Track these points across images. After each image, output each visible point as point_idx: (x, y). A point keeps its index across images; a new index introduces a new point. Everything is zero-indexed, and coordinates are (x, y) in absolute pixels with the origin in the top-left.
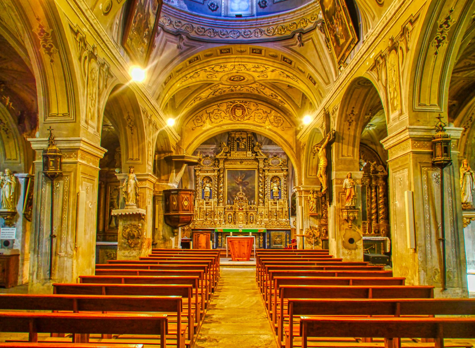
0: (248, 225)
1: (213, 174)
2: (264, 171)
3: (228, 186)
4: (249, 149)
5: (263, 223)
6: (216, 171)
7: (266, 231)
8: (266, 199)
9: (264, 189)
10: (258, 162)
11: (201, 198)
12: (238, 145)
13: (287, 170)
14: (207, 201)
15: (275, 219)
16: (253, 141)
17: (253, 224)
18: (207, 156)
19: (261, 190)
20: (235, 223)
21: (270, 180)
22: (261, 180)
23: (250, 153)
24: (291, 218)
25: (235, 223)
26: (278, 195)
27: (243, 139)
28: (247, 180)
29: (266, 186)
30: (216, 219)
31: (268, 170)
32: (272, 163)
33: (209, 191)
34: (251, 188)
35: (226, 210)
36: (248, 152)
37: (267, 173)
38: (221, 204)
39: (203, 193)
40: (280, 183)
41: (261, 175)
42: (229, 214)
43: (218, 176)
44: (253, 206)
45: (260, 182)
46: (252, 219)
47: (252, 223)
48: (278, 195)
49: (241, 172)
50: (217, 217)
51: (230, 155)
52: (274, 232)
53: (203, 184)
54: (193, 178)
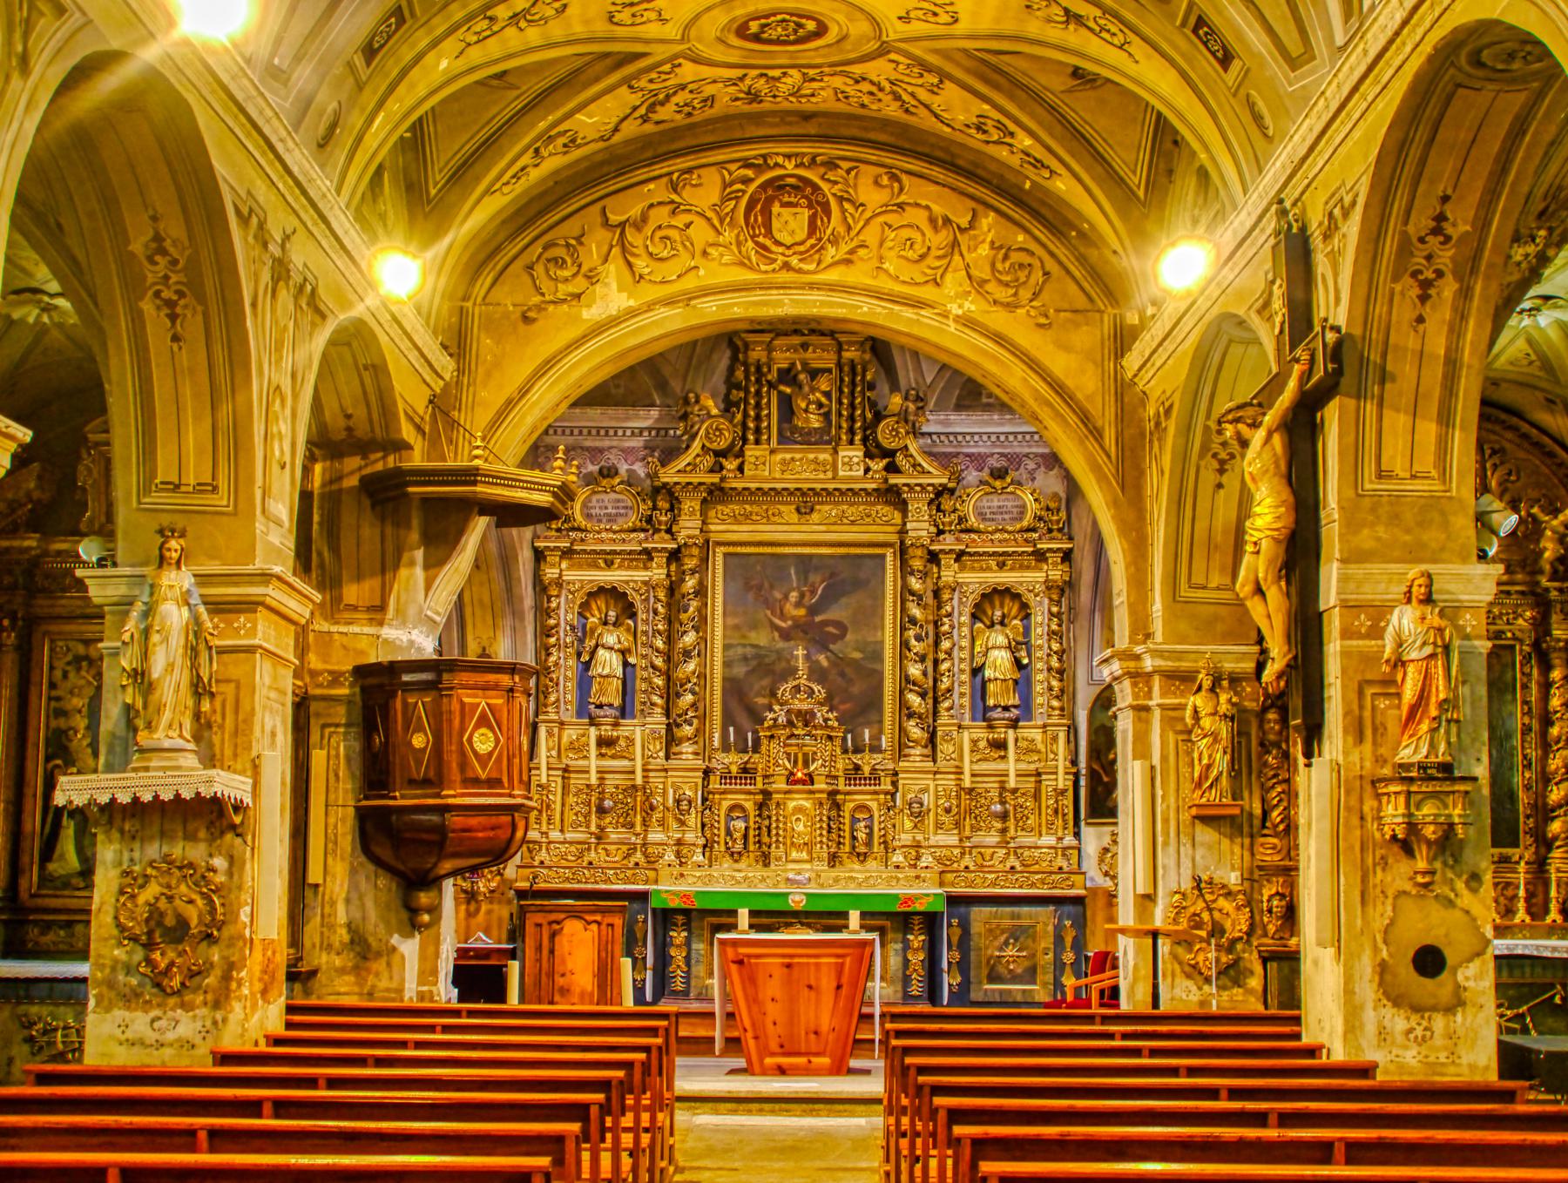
0: (838, 872)
1: (641, 575)
2: (933, 558)
3: (726, 647)
5: (926, 860)
6: (658, 559)
7: (941, 906)
8: (944, 718)
10: (902, 506)
11: (568, 715)
12: (787, 410)
13: (1067, 556)
14: (607, 731)
15: (993, 839)
16: (871, 387)
17: (872, 864)
18: (609, 472)
19: (915, 671)
20: (765, 860)
21: (967, 610)
22: (916, 612)
23: (857, 453)
24: (1088, 832)
25: (765, 860)
27: (814, 374)
29: (946, 645)
30: (655, 836)
31: (960, 556)
32: (981, 516)
33: (619, 672)
34: (857, 655)
35: (715, 784)
40: (1027, 631)
41: (915, 583)
42: (732, 808)
43: (672, 590)
44: (867, 761)
45: (913, 621)
46: (861, 836)
47: (863, 857)
49: (805, 563)
51: (741, 469)
52: (987, 910)
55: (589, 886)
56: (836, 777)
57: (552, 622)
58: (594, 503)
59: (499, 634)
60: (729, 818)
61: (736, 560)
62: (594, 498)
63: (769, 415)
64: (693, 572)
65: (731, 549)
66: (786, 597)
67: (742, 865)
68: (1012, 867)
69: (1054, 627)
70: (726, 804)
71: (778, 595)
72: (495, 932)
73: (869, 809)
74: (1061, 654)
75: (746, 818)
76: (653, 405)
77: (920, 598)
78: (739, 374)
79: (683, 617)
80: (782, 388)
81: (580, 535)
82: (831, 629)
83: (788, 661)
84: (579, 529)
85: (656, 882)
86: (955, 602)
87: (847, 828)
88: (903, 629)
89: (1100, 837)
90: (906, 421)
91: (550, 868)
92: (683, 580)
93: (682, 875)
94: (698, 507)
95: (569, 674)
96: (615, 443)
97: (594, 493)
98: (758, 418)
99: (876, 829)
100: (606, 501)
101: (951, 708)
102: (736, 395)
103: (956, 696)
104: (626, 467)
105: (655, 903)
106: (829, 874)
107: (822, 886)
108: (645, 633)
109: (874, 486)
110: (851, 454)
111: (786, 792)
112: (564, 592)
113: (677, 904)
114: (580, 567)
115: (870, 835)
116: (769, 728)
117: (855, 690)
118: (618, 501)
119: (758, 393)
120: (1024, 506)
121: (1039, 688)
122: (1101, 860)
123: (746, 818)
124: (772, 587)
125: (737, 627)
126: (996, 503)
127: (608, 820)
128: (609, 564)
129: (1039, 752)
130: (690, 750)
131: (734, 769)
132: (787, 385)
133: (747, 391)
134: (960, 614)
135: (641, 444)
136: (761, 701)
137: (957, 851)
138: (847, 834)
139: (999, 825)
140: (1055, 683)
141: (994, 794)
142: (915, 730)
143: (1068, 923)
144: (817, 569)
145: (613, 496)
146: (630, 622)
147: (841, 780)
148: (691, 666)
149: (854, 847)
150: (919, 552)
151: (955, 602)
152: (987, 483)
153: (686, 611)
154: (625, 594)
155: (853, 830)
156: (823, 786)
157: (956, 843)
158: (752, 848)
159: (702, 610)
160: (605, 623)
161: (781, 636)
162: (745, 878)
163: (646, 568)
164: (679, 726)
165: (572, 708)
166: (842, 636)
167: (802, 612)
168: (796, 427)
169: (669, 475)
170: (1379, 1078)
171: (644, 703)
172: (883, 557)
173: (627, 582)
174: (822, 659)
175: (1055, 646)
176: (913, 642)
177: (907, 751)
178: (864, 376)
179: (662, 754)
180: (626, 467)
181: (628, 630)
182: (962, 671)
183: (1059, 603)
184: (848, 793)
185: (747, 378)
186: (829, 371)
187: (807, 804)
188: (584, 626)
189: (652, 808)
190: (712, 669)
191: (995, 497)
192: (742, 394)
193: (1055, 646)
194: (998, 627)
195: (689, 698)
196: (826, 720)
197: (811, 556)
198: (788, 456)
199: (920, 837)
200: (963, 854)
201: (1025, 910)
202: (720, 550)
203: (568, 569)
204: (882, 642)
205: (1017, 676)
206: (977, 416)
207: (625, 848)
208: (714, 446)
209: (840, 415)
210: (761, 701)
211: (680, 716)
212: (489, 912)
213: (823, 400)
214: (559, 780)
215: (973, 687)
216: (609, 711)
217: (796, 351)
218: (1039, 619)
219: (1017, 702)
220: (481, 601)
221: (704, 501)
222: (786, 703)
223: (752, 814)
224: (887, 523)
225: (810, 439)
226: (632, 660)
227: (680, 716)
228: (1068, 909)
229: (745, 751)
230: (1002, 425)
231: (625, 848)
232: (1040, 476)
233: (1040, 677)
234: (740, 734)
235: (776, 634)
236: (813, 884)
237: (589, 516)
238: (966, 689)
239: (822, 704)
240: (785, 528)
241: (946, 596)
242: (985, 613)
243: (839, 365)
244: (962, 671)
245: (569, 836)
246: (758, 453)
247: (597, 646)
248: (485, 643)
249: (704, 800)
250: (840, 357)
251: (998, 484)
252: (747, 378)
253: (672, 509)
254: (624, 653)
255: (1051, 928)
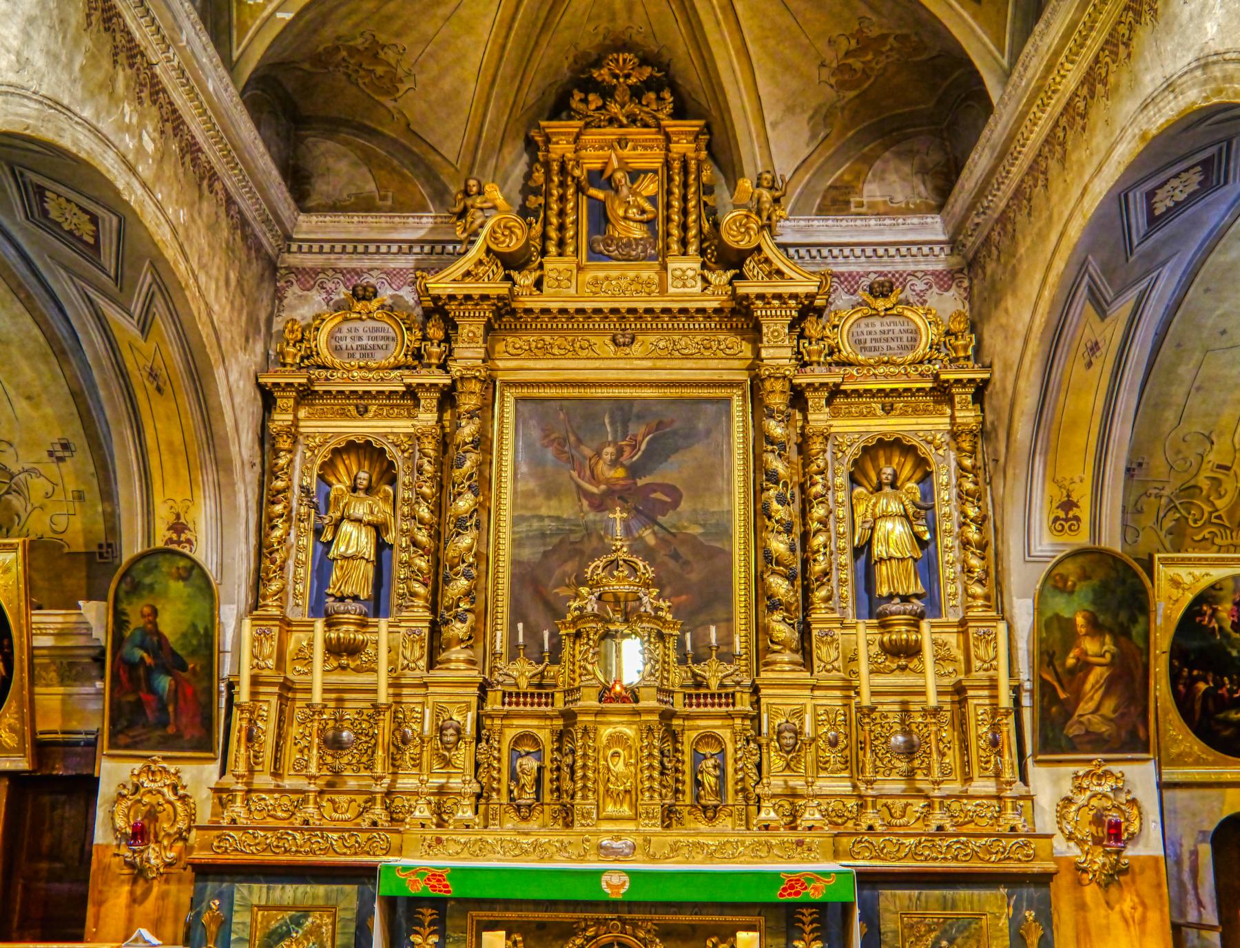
0: (674, 836)
1: (403, 426)
2: (798, 398)
3: (516, 521)
4: (684, 243)
5: (811, 816)
6: (429, 401)
7: (848, 893)
8: (819, 612)
9: (805, 537)
10: (754, 332)
11: (297, 611)
12: (600, 218)
13: (980, 392)
14: (347, 632)
15: (896, 786)
16: (709, 190)
17: (725, 823)
18: (363, 294)
19: (778, 545)
20: (567, 816)
21: (845, 469)
22: (778, 466)
23: (689, 265)
24: (1039, 775)
25: (567, 816)
26: (915, 587)
27: (634, 175)
28: (670, 472)
29: (819, 512)
30: (407, 782)
31: (835, 392)
32: (860, 344)
33: (369, 551)
34: (696, 530)
35: (494, 703)
36: (676, 264)
37: (819, 417)
38: (457, 654)
39: (322, 569)
40: (928, 494)
41: (775, 429)
42: (518, 740)
43: (444, 443)
44: (714, 673)
45: (774, 477)
46: (709, 780)
47: (711, 813)
48: (915, 587)
49: (624, 412)
50: (417, 764)
51: (538, 284)
52: (904, 895)
53: (320, 501)
54: (243, 446)
55: (301, 858)
56: (670, 693)
57: (280, 484)
58: (345, 333)
59: (198, 494)
60: (515, 754)
61: (530, 406)
62: (345, 326)
63: (576, 222)
64: (471, 415)
65: (525, 392)
66: (599, 454)
67: (533, 825)
68: (940, 828)
69: (969, 486)
70: (510, 734)
71: (588, 452)
72: (168, 930)
73: (719, 741)
74: (981, 522)
75: (539, 755)
76: (424, 209)
77: (783, 446)
78: (539, 176)
79: (457, 473)
80: (593, 192)
81: (324, 373)
82: (658, 495)
83: (601, 538)
84: (324, 367)
85: (400, 851)
86: (828, 455)
87: (687, 768)
88: (759, 491)
89: (1056, 781)
90: (759, 213)
91: (244, 829)
92: (459, 426)
93: (439, 841)
94: (481, 332)
95: (302, 557)
96: (377, 264)
97: (346, 320)
98: (562, 228)
99: (730, 770)
100: (360, 332)
101: (828, 599)
102: (533, 202)
103: (834, 583)
104: (390, 292)
105: (385, 887)
106: (665, 838)
107: (653, 858)
108: (406, 501)
109: (716, 305)
110: (684, 266)
111: (597, 714)
112: (300, 448)
113: (420, 889)
114: (322, 416)
115: (722, 779)
116: (574, 622)
117: (694, 577)
118: (377, 330)
119: (562, 199)
120: (917, 331)
121: (949, 573)
122: (1061, 817)
123: (539, 755)
124: (579, 441)
125: (530, 495)
126: (878, 328)
127: (345, 760)
128: (362, 412)
129: (954, 660)
130: (462, 656)
131: (523, 683)
132: (600, 187)
133: (548, 194)
134: (835, 474)
135: (411, 265)
136: (563, 592)
137: (851, 803)
138: (688, 778)
139: (903, 765)
140: (974, 562)
141: (894, 719)
142: (782, 627)
143: (1030, 915)
144: (640, 417)
145: (371, 324)
146: (389, 489)
147: (679, 699)
148: (466, 541)
149: (698, 797)
150: (779, 386)
151: (828, 455)
152: (864, 303)
153: (460, 466)
154: (382, 452)
155: (696, 772)
156: (653, 704)
157: (849, 790)
158: (547, 798)
159: (483, 465)
160: (354, 489)
161: (591, 505)
162: (535, 845)
163: (411, 417)
164: (447, 623)
165: (305, 602)
166: (675, 504)
167: (620, 473)
168: (612, 238)
169: (441, 285)
170: (851, 899)
171: (402, 596)
172: (728, 401)
173: (385, 435)
174: (648, 536)
175: (972, 512)
176: (775, 506)
177: (770, 657)
178: (698, 178)
179: (422, 663)
180: (390, 292)
181: (386, 499)
182: (842, 551)
183: (973, 453)
184: (687, 717)
185: (548, 179)
186: (655, 172)
187: (630, 732)
188: (328, 495)
189: (405, 741)
190: (497, 549)
191: (877, 321)
192: (541, 200)
193: (972, 512)
194: (887, 489)
195: (463, 583)
196: (657, 609)
197: (631, 401)
198: (601, 274)
199: (798, 783)
200: (862, 806)
201: (963, 894)
202: (510, 395)
203: (308, 418)
204: (730, 512)
205: (919, 554)
206: (846, 222)
207: (360, 799)
208: (502, 248)
209: (669, 234)
210: (563, 592)
211: (448, 609)
212: (163, 896)
213: (647, 206)
214: (274, 700)
215: (855, 571)
216: (352, 606)
217: (612, 147)
218: (944, 479)
219: (920, 589)
220: (170, 444)
221: (489, 328)
222: (598, 584)
223: (548, 748)
224: (734, 357)
225: (627, 253)
226: (389, 538)
227: (448, 609)
228: (1028, 892)
229: (540, 662)
230: (880, 232)
231: (360, 799)
232: (933, 298)
233: (950, 557)
234: (533, 634)
235: (585, 503)
236: (639, 855)
237: (337, 350)
238: (846, 574)
239: (647, 586)
240: (597, 364)
241: (816, 447)
242: (866, 476)
243: (667, 164)
244: (842, 551)
245: (287, 783)
246: (561, 267)
247: (342, 519)
248: (179, 508)
249: (479, 726)
250: (668, 150)
251: (880, 304)
252: (548, 179)
253: (447, 339)
254: (379, 529)
255: (1004, 922)
